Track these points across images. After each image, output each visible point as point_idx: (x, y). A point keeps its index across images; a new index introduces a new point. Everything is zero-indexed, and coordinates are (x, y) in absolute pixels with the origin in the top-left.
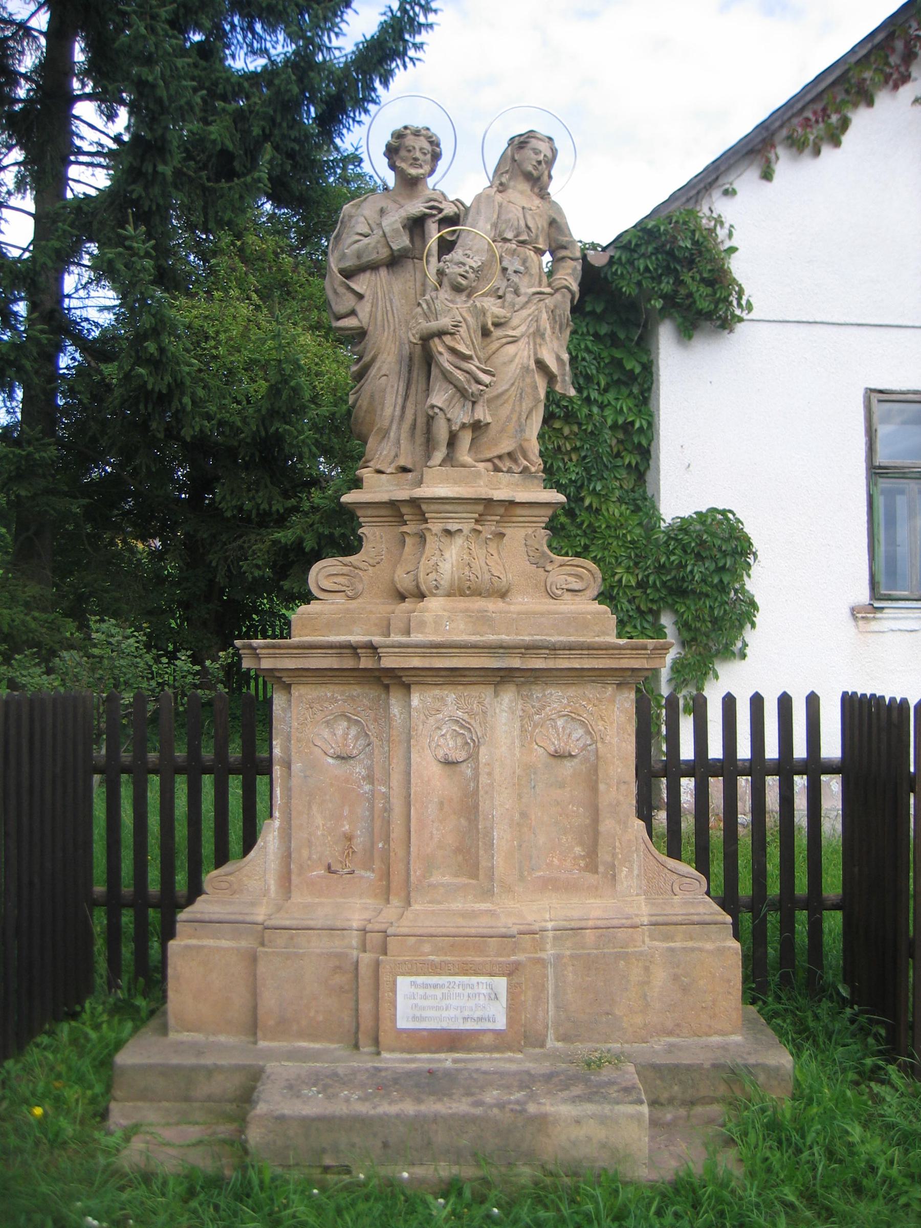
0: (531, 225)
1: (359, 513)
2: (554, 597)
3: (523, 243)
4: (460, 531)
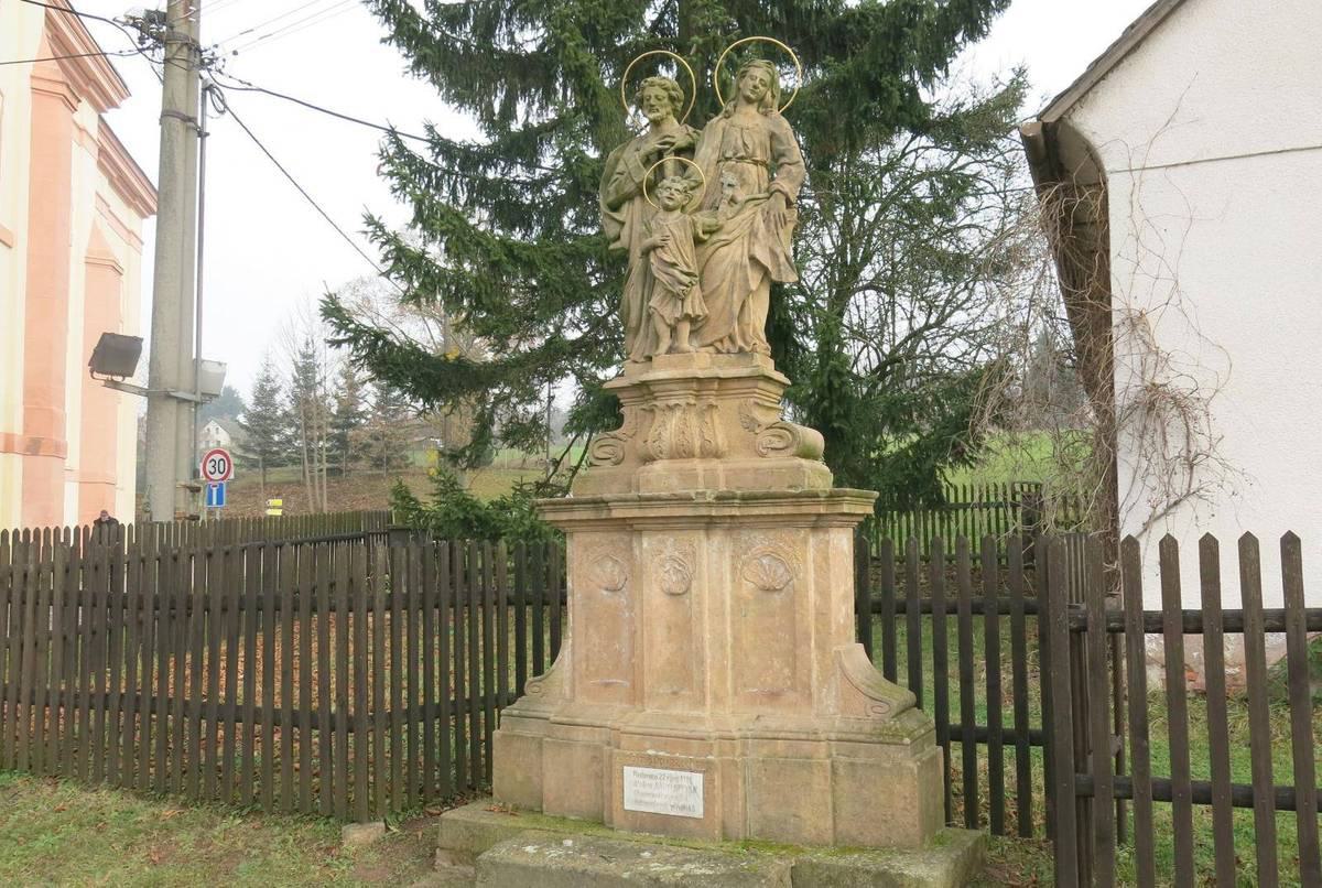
2: (763, 456)
3: (742, 158)
4: (677, 405)
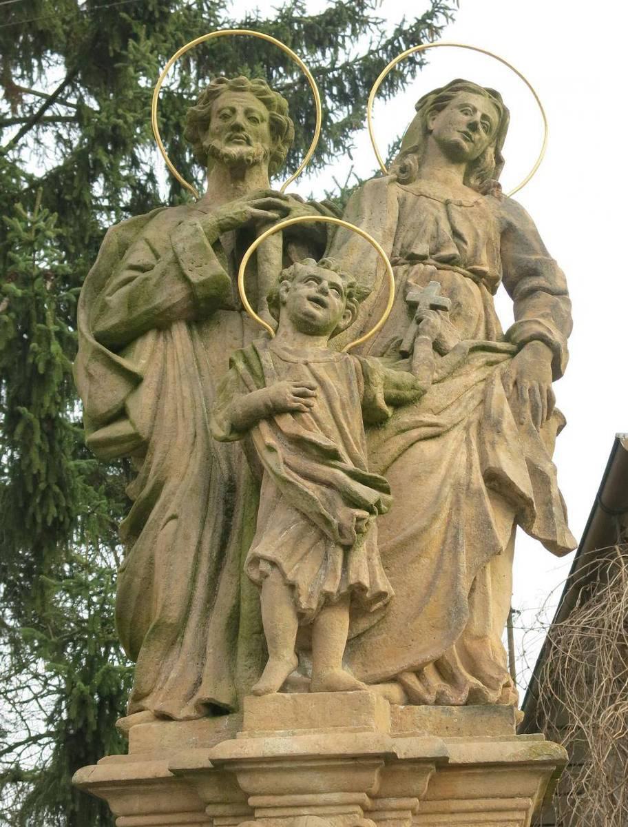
0: (463, 229)
1: (115, 807)
3: (450, 261)
